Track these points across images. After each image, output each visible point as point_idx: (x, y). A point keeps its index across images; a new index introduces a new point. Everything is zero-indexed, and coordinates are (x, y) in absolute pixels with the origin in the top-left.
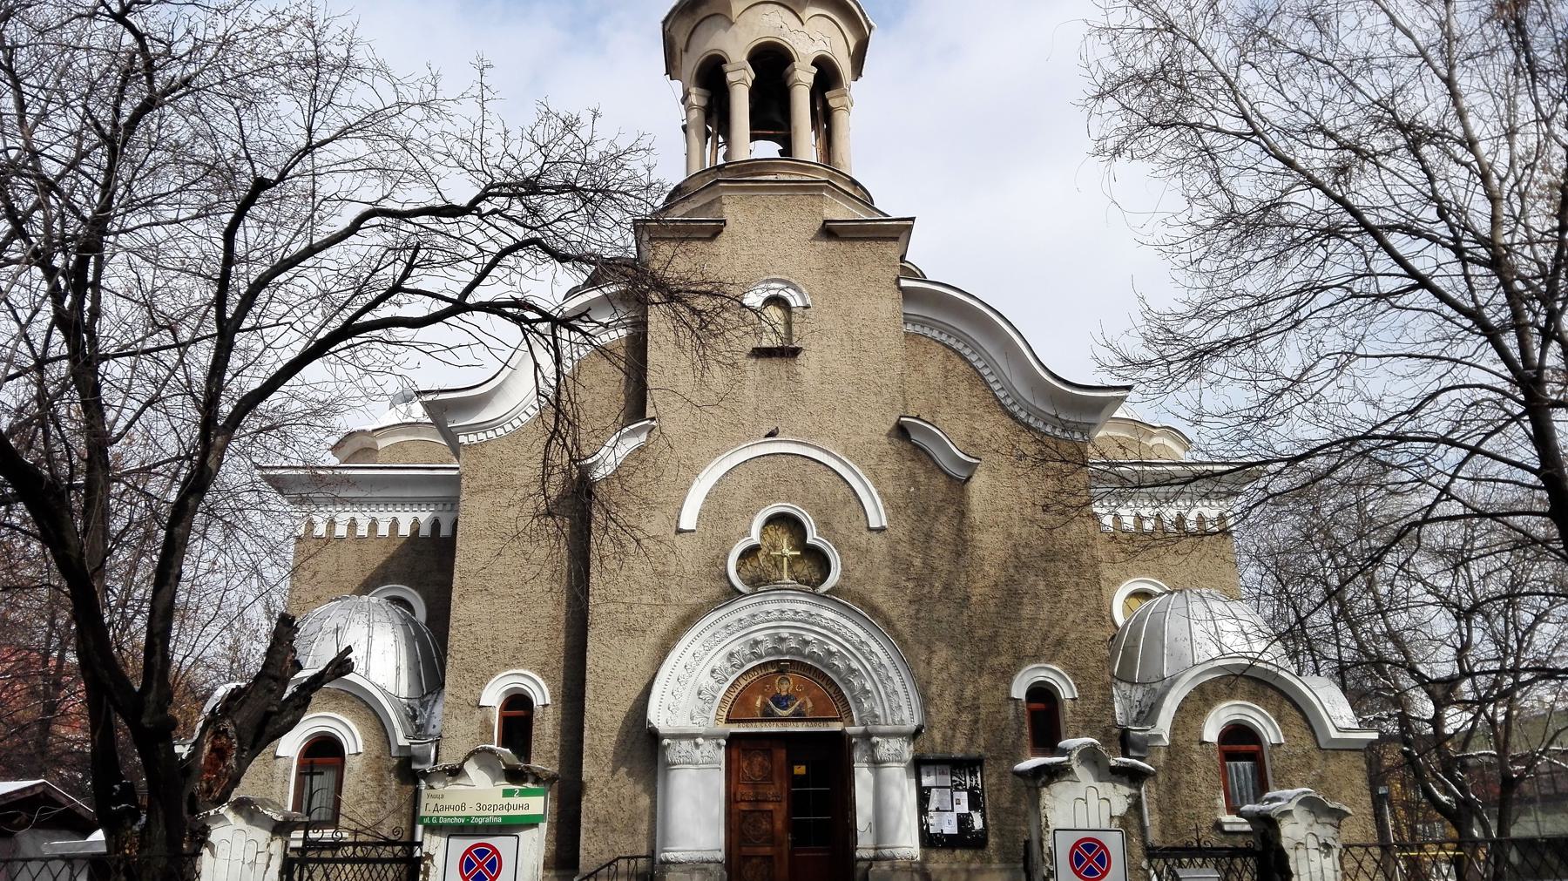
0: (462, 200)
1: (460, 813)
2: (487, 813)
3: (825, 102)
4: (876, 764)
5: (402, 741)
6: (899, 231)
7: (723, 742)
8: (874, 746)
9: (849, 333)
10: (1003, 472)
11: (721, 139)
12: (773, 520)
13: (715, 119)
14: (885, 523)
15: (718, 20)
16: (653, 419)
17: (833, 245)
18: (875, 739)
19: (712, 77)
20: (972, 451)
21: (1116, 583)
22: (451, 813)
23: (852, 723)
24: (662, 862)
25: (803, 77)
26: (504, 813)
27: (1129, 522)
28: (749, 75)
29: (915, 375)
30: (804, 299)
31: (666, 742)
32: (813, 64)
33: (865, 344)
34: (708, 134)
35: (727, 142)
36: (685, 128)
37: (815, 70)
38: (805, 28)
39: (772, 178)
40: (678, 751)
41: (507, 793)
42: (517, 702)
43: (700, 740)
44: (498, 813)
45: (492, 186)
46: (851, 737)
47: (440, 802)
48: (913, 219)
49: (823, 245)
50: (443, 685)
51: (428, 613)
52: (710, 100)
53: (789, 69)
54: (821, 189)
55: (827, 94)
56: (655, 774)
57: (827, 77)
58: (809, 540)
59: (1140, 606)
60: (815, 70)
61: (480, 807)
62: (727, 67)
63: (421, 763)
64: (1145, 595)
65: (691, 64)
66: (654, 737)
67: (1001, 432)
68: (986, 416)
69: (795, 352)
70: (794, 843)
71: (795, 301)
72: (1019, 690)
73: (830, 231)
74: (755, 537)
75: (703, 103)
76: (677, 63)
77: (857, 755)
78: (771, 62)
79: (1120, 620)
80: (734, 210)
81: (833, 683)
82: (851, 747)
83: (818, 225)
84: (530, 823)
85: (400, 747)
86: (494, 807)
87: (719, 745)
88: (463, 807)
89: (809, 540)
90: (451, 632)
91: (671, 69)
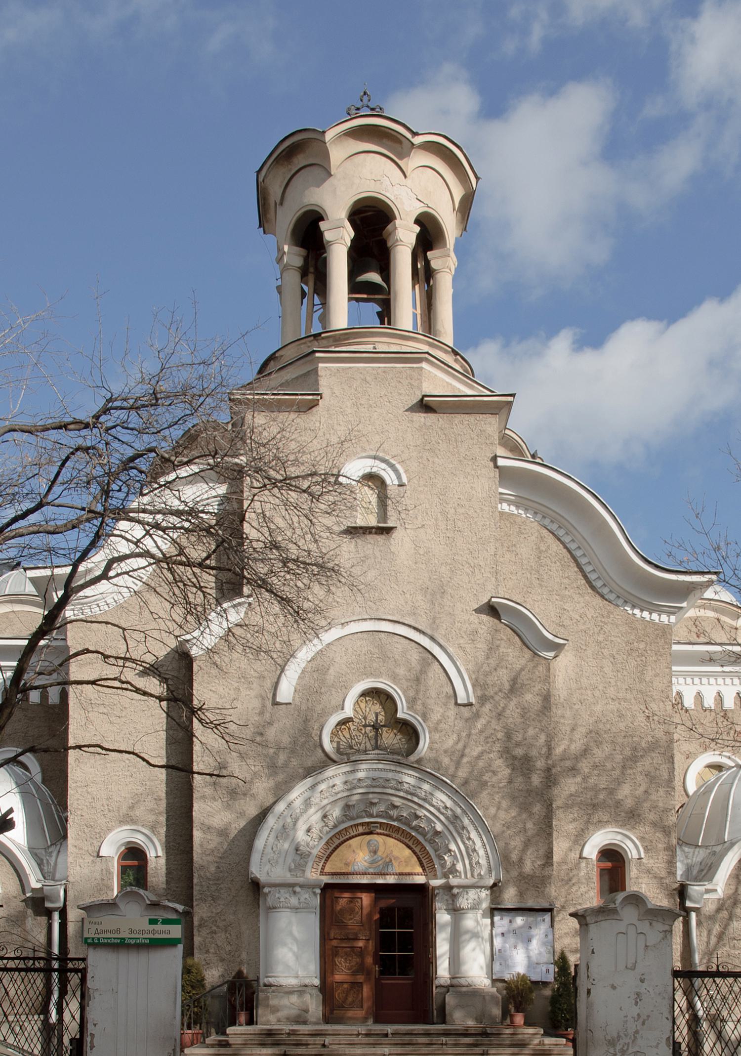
0: (85, 415)
1: (116, 936)
2: (137, 936)
3: (427, 262)
4: (456, 911)
5: (35, 885)
6: (501, 408)
7: (318, 891)
8: (454, 897)
9: (444, 513)
10: (589, 652)
11: (317, 301)
12: (365, 694)
13: (311, 278)
14: (473, 700)
15: (315, 170)
16: (248, 597)
17: (432, 416)
18: (455, 891)
19: (309, 234)
20: (561, 632)
21: (690, 757)
22: (109, 935)
23: (435, 877)
24: (265, 985)
25: (404, 236)
26: (151, 936)
27: (709, 702)
28: (348, 233)
29: (508, 556)
30: (399, 477)
31: (266, 890)
32: (418, 221)
33: (459, 524)
34: (303, 294)
35: (324, 303)
36: (279, 289)
37: (417, 229)
38: (408, 182)
39: (369, 348)
40: (273, 897)
41: (153, 922)
42: (134, 855)
43: (298, 889)
44: (146, 936)
45: (110, 400)
46: (434, 888)
47: (99, 927)
48: (513, 395)
49: (421, 418)
50: (65, 837)
51: (44, 771)
52: (306, 259)
53: (390, 227)
54: (420, 360)
55: (428, 253)
56: (258, 915)
57: (429, 235)
58: (400, 715)
59: (712, 775)
60: (417, 229)
61: (132, 931)
62: (323, 225)
63: (52, 902)
64: (719, 767)
65: (286, 219)
66: (256, 886)
67: (590, 613)
68: (576, 597)
69: (388, 531)
70: (382, 973)
71: (390, 478)
72: (591, 850)
73: (425, 406)
74: (348, 711)
75: (298, 262)
76: (271, 214)
77: (438, 905)
78: (372, 221)
79: (692, 788)
80: (329, 373)
81: (419, 843)
82: (434, 896)
83: (415, 399)
84: (170, 943)
85: (33, 890)
86: (143, 932)
87: (314, 893)
88: (118, 931)
89: (400, 715)
90: (70, 792)
91: (264, 219)
